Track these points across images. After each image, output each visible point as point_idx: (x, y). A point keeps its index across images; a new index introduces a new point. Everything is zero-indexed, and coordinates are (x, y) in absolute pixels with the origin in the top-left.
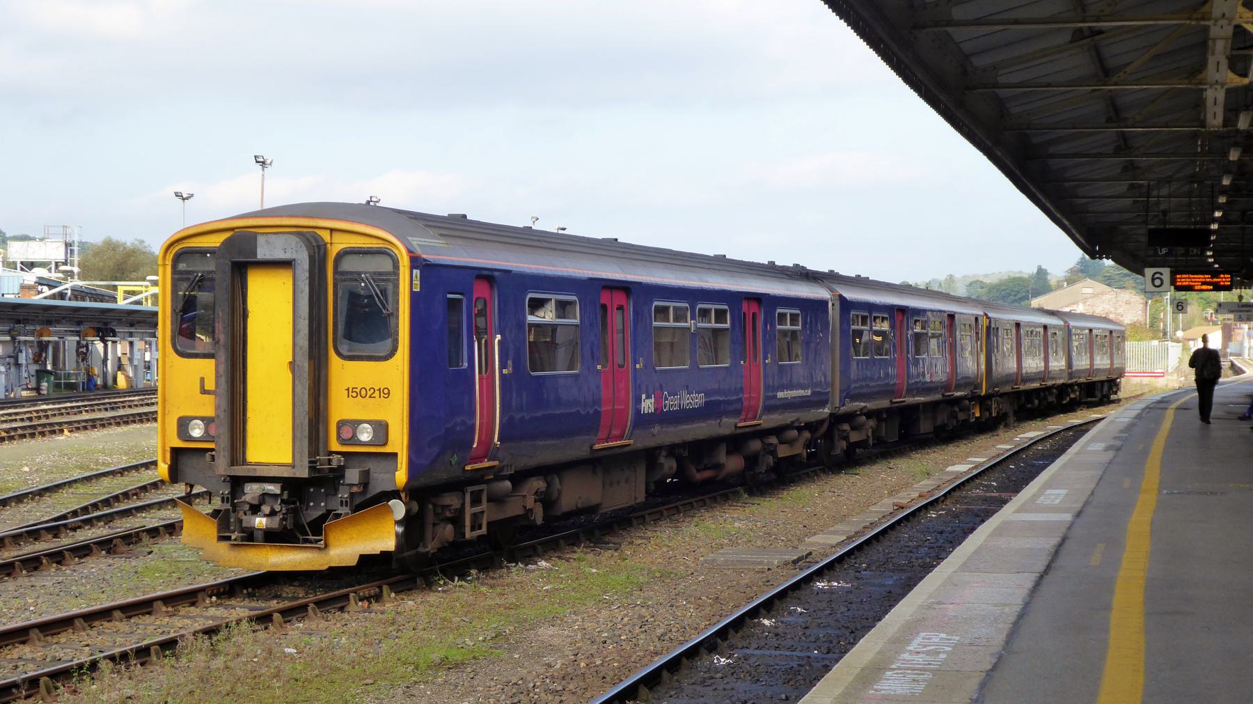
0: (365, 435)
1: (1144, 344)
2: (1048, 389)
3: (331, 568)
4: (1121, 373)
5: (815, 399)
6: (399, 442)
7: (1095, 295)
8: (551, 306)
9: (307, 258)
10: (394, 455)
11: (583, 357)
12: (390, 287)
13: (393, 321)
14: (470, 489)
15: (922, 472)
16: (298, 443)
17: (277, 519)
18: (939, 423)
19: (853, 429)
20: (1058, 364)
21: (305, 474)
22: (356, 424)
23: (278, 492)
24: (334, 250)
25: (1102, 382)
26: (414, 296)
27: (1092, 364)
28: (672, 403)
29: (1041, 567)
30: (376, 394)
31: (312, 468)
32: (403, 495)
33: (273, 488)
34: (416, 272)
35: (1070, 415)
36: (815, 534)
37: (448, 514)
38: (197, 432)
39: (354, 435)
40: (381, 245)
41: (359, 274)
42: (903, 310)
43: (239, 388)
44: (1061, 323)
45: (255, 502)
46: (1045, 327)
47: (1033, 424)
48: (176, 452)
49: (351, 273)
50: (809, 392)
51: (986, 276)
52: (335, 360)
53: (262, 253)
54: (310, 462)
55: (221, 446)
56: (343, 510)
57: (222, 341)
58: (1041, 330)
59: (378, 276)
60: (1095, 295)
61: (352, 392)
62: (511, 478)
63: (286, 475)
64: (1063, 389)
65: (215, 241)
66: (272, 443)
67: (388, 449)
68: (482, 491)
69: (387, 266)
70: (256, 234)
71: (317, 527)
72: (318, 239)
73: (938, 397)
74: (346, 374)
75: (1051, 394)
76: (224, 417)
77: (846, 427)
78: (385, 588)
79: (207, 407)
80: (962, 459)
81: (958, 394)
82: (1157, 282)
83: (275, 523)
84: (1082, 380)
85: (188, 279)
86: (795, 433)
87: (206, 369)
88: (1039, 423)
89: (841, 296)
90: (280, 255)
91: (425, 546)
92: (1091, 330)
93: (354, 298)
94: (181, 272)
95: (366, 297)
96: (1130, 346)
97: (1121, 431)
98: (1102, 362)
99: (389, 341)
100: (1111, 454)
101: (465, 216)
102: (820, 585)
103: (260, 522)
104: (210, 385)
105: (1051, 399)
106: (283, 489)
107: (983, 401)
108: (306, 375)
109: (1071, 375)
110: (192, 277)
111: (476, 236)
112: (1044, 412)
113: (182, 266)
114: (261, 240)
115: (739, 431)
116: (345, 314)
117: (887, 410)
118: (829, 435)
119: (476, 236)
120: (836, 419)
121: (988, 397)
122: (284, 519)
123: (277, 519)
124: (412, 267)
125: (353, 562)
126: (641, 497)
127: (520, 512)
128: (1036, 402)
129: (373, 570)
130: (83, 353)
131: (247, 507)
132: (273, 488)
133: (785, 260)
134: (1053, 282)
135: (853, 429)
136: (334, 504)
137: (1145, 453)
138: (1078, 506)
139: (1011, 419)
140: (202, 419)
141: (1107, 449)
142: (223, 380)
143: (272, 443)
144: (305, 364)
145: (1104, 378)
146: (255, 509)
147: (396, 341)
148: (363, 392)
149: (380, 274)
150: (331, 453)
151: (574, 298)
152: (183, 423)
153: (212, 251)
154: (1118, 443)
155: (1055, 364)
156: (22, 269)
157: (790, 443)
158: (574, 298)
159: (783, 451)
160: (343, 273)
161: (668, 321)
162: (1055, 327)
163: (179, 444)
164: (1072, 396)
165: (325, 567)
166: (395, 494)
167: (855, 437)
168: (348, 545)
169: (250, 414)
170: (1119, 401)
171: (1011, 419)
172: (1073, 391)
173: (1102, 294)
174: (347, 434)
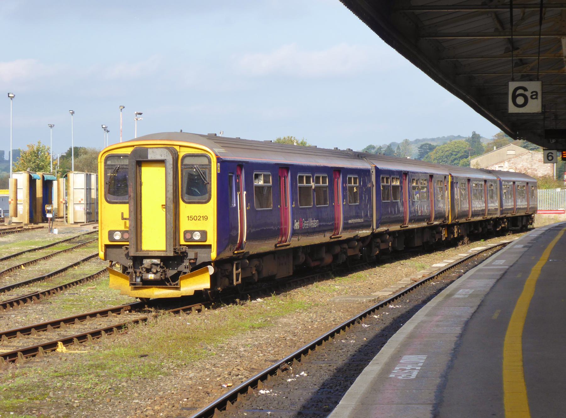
0: (197, 236)
1: (550, 191)
2: (488, 221)
3: (182, 296)
4: (535, 210)
5: (365, 224)
6: (212, 239)
7: (516, 156)
8: (262, 178)
9: (172, 159)
10: (209, 246)
12: (207, 171)
13: (208, 185)
14: (236, 262)
15: (420, 267)
16: (168, 241)
17: (159, 274)
18: (425, 240)
20: (494, 205)
21: (171, 254)
22: (192, 232)
23: (159, 263)
24: (181, 155)
25: (522, 216)
26: (219, 175)
27: (515, 204)
28: (306, 225)
29: (498, 277)
30: (201, 218)
31: (175, 252)
32: (212, 264)
34: (219, 164)
35: (502, 238)
36: (375, 292)
37: (227, 274)
38: (117, 236)
39: (192, 237)
40: (202, 152)
41: (193, 165)
42: (406, 174)
43: (139, 217)
44: (495, 178)
45: (149, 267)
46: (485, 181)
47: (478, 243)
48: (107, 246)
49: (189, 165)
50: (362, 220)
51: (433, 140)
52: (182, 204)
53: (151, 157)
54: (174, 249)
55: (130, 244)
56: (187, 270)
57: (132, 196)
58: (483, 183)
60: (516, 156)
61: (190, 218)
63: (163, 255)
64: (497, 221)
65: (129, 151)
66: (155, 240)
67: (207, 243)
68: (377, 227)
69: (205, 161)
70: (147, 148)
71: (175, 278)
72: (175, 150)
73: (425, 224)
74: (186, 210)
75: (489, 224)
76: (133, 230)
77: (379, 240)
78: (203, 306)
80: (442, 260)
81: (436, 223)
82: (550, 158)
83: (158, 276)
84: (509, 215)
85: (112, 168)
87: (125, 209)
88: (482, 242)
89: (376, 167)
90: (159, 157)
92: (514, 183)
93: (191, 176)
94: (109, 165)
95: (196, 176)
96: (541, 193)
97: (532, 240)
98: (522, 203)
99: (207, 195)
100: (526, 249)
101: (216, 135)
102: (391, 306)
103: (151, 276)
104: (126, 215)
105: (489, 227)
106: (161, 262)
107: (450, 228)
108: (172, 211)
109: (502, 212)
110: (114, 167)
112: (486, 236)
113: (109, 163)
115: (333, 240)
116: (188, 184)
117: (398, 232)
118: (369, 246)
119: (234, 146)
120: (374, 235)
121: (452, 225)
122: (161, 275)
123: (159, 274)
124: (217, 162)
125: (192, 293)
126: (291, 274)
127: (250, 275)
128: (480, 229)
129: (199, 298)
131: (144, 270)
133: (343, 147)
134: (484, 144)
135: (382, 242)
136: (181, 268)
137: (545, 248)
138: (511, 264)
139: (466, 239)
140: (120, 231)
141: (524, 247)
142: (133, 214)
144: (172, 206)
145: (523, 214)
146: (148, 271)
147: (210, 195)
148: (195, 218)
149: (203, 165)
150: (181, 245)
151: (326, 175)
153: (125, 156)
154: (530, 245)
155: (492, 205)
157: (353, 248)
158: (269, 173)
159: (350, 253)
160: (185, 165)
162: (491, 181)
163: (109, 243)
164: (503, 226)
165: (180, 296)
166: (209, 263)
167: (383, 246)
168: (190, 286)
169: (143, 228)
170: (534, 228)
171: (466, 239)
172: (504, 223)
173: (522, 154)
174: (188, 236)
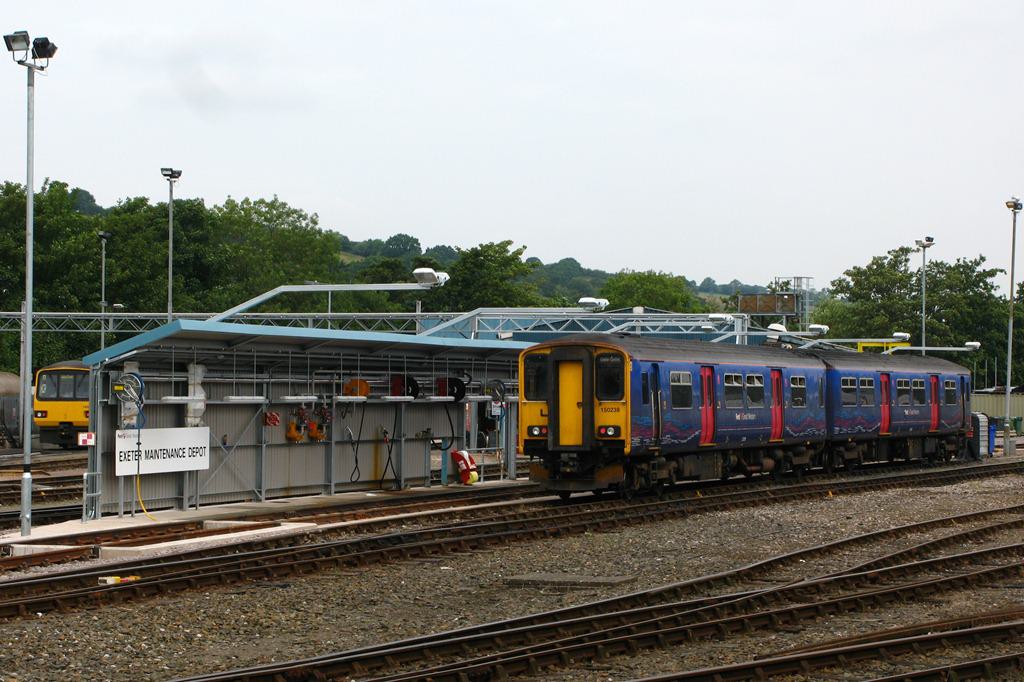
19: (847, 450)
22: (606, 428)
24: (595, 355)
33: (575, 455)
39: (606, 432)
59: (615, 364)
66: (571, 433)
77: (842, 449)
79: (544, 421)
86: (804, 448)
104: (545, 412)
130: (320, 397)
132: (575, 455)
143: (571, 433)
146: (566, 464)
152: (530, 429)
156: (332, 328)
161: (1011, 385)
163: (527, 438)
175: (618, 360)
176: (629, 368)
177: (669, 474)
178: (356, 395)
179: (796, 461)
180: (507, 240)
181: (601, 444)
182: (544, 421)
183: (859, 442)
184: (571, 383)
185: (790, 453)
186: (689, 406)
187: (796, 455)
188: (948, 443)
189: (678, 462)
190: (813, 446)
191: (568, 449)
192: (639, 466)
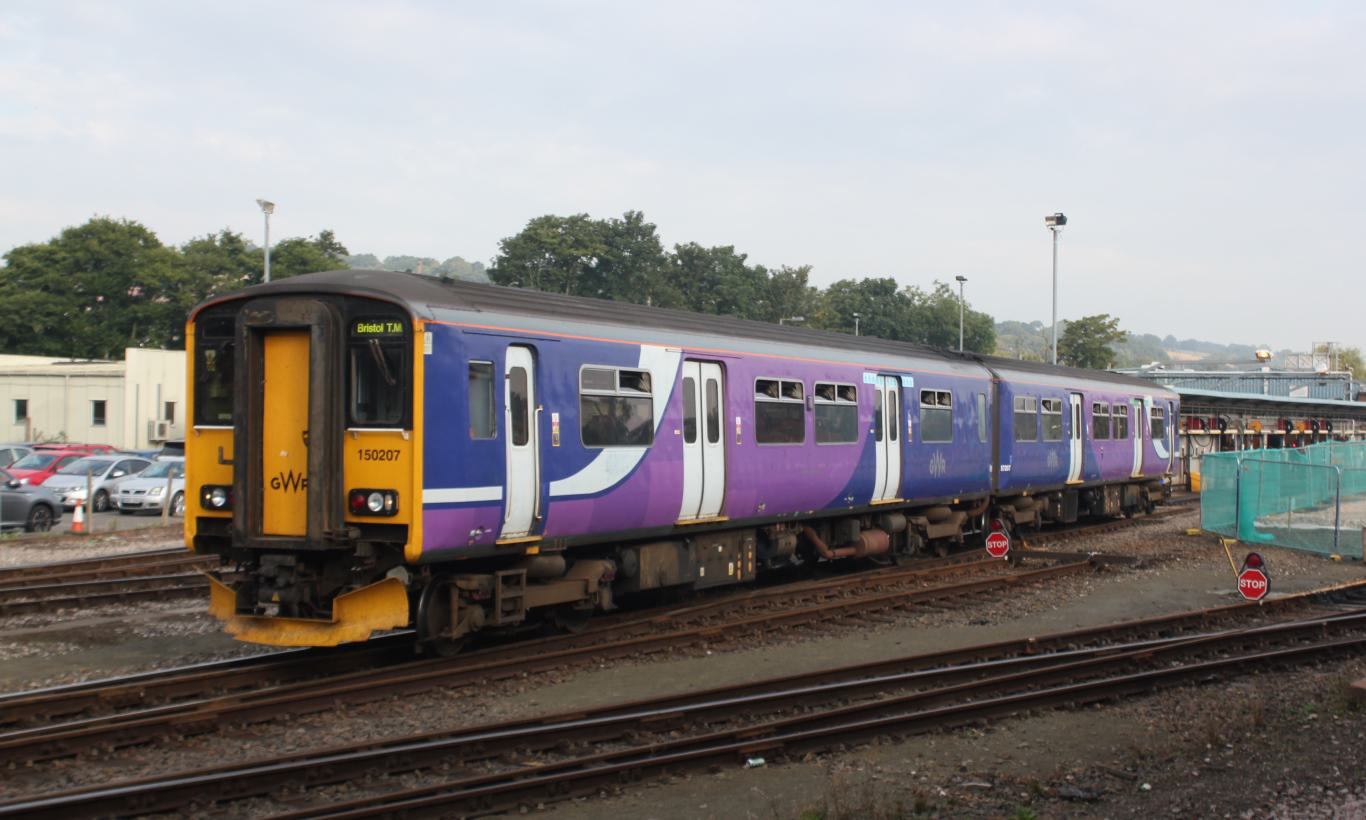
11: (376, 349)
22: (367, 493)
33: (290, 560)
59: (397, 337)
62: (564, 554)
77: (1011, 508)
79: (225, 475)
91: (450, 631)
104: (229, 455)
106: (299, 561)
111: (511, 303)
114: (426, 353)
119: (511, 303)
129: (382, 650)
132: (290, 560)
175: (398, 328)
176: (424, 345)
177: (1036, 516)
178: (695, 419)
179: (934, 532)
180: (1105, 314)
181: (354, 533)
182: (225, 475)
183: (1036, 496)
184: (287, 379)
185: (922, 520)
186: (855, 440)
187: (933, 522)
188: (1151, 491)
189: (619, 561)
190: (965, 506)
191: (281, 547)
192: (461, 584)
